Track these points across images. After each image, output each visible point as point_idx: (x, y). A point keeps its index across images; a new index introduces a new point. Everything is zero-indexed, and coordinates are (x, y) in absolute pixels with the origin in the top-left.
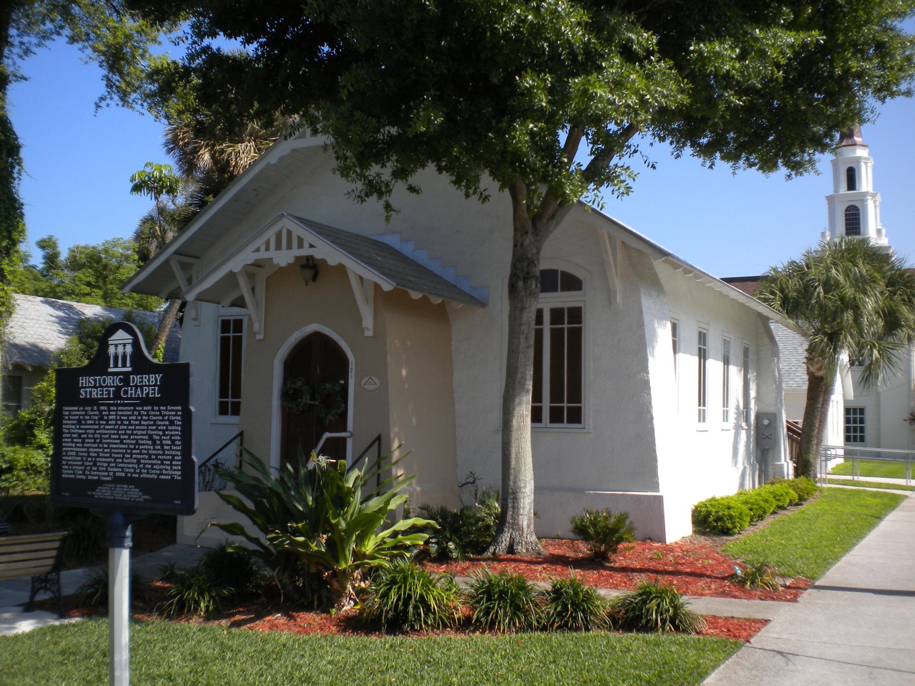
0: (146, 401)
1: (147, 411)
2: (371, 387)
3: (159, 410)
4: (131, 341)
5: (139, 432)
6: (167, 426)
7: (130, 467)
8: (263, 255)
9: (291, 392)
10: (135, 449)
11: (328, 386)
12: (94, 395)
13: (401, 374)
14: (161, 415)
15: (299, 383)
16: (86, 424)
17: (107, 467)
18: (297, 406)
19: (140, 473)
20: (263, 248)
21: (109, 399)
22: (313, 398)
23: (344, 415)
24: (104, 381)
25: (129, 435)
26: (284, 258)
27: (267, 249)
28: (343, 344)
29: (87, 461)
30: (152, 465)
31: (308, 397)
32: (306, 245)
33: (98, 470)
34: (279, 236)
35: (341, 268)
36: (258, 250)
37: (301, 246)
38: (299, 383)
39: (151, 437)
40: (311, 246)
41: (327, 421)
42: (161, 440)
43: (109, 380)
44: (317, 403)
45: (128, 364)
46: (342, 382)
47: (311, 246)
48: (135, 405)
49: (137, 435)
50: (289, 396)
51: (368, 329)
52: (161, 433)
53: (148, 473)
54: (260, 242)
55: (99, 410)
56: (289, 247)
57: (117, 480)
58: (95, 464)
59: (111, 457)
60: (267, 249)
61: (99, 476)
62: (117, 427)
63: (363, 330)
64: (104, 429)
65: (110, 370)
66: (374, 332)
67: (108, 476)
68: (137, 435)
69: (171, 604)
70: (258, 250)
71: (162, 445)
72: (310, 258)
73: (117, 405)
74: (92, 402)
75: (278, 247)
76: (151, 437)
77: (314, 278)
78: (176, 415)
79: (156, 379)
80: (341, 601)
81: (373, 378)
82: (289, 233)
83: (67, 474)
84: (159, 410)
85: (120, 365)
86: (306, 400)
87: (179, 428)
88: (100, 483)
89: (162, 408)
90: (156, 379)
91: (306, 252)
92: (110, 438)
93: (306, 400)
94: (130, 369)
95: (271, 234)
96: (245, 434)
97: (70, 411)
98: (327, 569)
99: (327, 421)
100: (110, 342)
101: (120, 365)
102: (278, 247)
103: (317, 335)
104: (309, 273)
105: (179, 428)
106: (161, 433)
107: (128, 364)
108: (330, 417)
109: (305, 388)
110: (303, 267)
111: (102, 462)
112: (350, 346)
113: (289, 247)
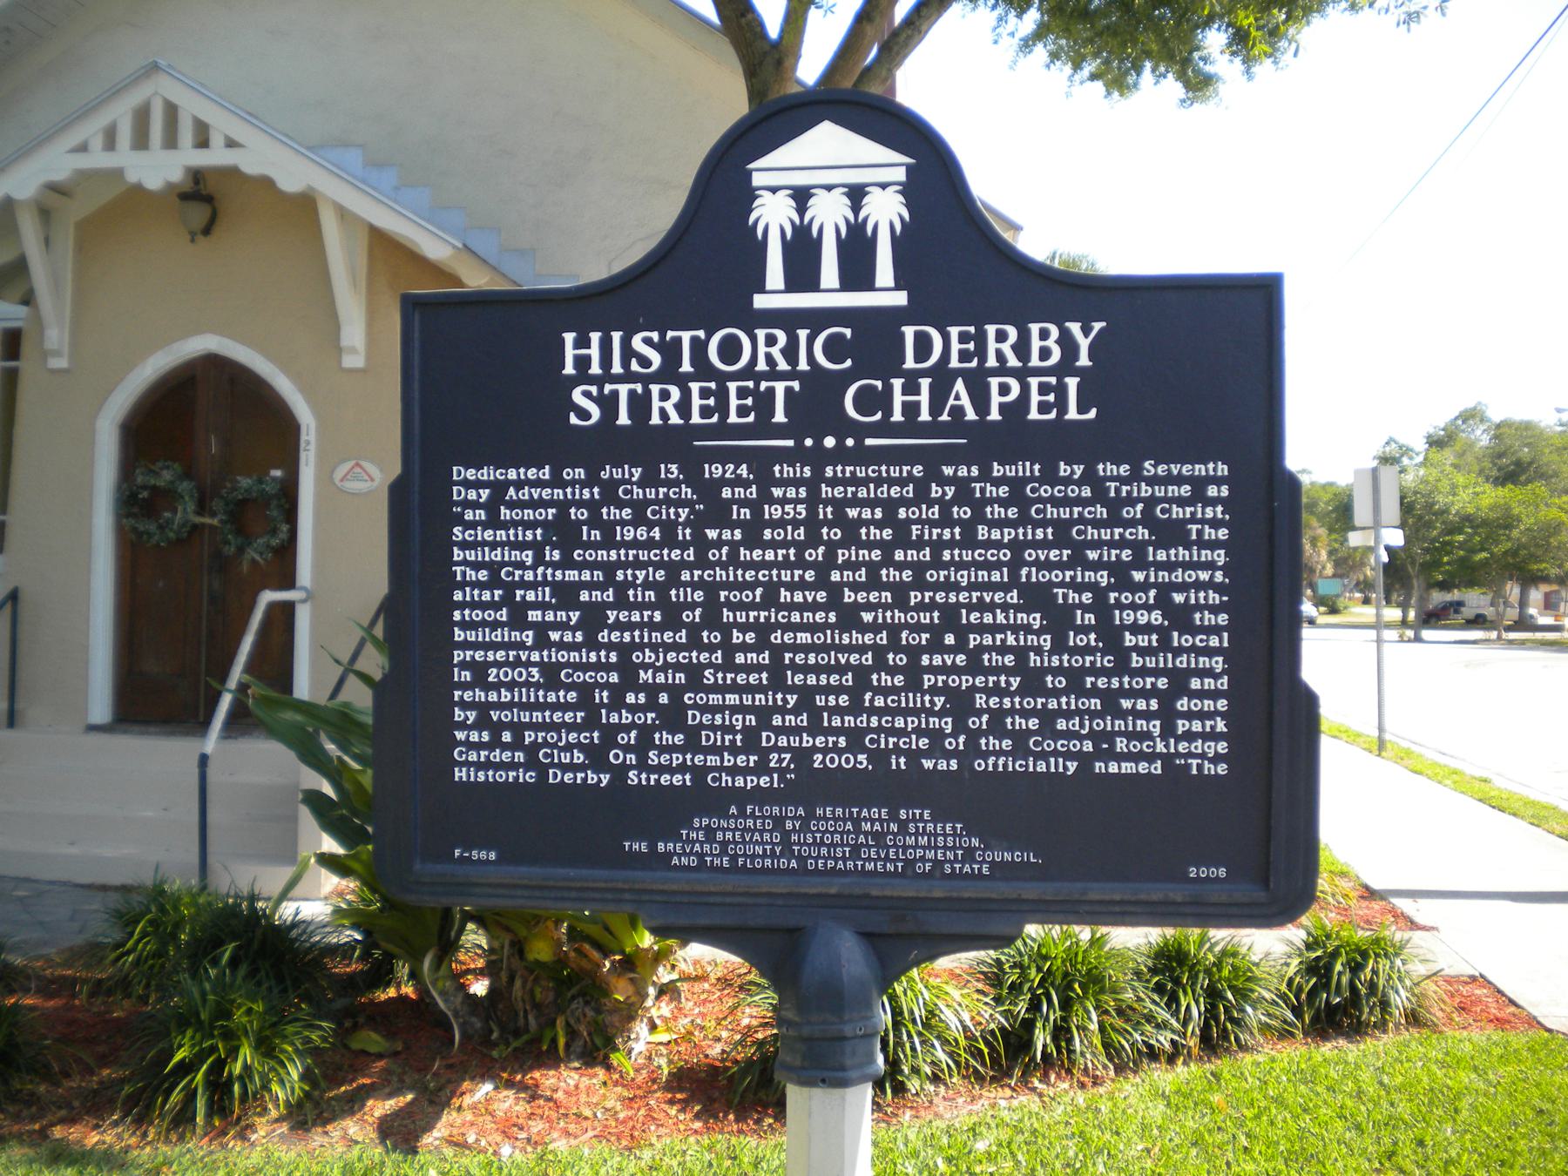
0: (1012, 436)
1: (1017, 484)
2: (351, 486)
3: (1098, 483)
4: (900, 175)
5: (963, 578)
6: (1138, 547)
7: (908, 729)
8: (99, 159)
9: (145, 494)
10: (936, 646)
11: (245, 482)
12: (664, 407)
13: (277, 467)
14: (1100, 496)
15: (167, 475)
16: (609, 542)
17: (751, 735)
18: (161, 527)
19: (973, 751)
20: (97, 143)
21: (765, 427)
22: (202, 508)
23: (286, 552)
24: (730, 350)
25: (900, 591)
26: (158, 169)
27: (110, 142)
28: (284, 385)
29: (617, 704)
30: (1047, 717)
31: (191, 507)
32: (217, 140)
33: (693, 745)
34: (142, 117)
35: (306, 204)
36: (83, 148)
37: (203, 143)
38: (167, 475)
39: (1037, 597)
40: (231, 144)
41: (245, 567)
42: (1101, 607)
43: (763, 348)
44: (215, 522)
45: (885, 271)
46: (277, 473)
47: (231, 144)
48: (932, 460)
49: (949, 586)
50: (135, 503)
51: (353, 350)
52: (1103, 578)
53: (1020, 750)
54: (91, 129)
55: (692, 475)
56: (171, 142)
57: (810, 787)
58: (673, 717)
59: (778, 683)
60: (110, 142)
61: (700, 772)
62: (817, 554)
63: (339, 350)
64: (734, 560)
65: (760, 302)
66: (369, 358)
67: (762, 768)
68: (949, 586)
69: (191, 1096)
70: (83, 148)
71: (1110, 636)
72: (197, 175)
73: (819, 458)
74: (648, 445)
75: (141, 141)
76: (1037, 597)
77: (207, 231)
78: (1198, 497)
79: (1067, 342)
80: (629, 1030)
81: (365, 464)
82: (171, 111)
83: (475, 762)
84: (1089, 478)
85: (830, 272)
86: (185, 512)
87: (1220, 557)
88: (708, 798)
89: (1105, 469)
90: (1067, 342)
91: (215, 157)
92: (770, 600)
93: (185, 512)
94: (900, 299)
95: (121, 113)
96: (22, 596)
97: (499, 488)
98: (606, 953)
99: (245, 567)
100: (758, 180)
101: (830, 272)
102: (141, 141)
103: (214, 363)
104: (199, 214)
105: (1220, 557)
106: (1103, 578)
107: (885, 271)
108: (252, 553)
109: (185, 486)
110: (185, 197)
111: (721, 712)
112: (302, 390)
113: (171, 142)
